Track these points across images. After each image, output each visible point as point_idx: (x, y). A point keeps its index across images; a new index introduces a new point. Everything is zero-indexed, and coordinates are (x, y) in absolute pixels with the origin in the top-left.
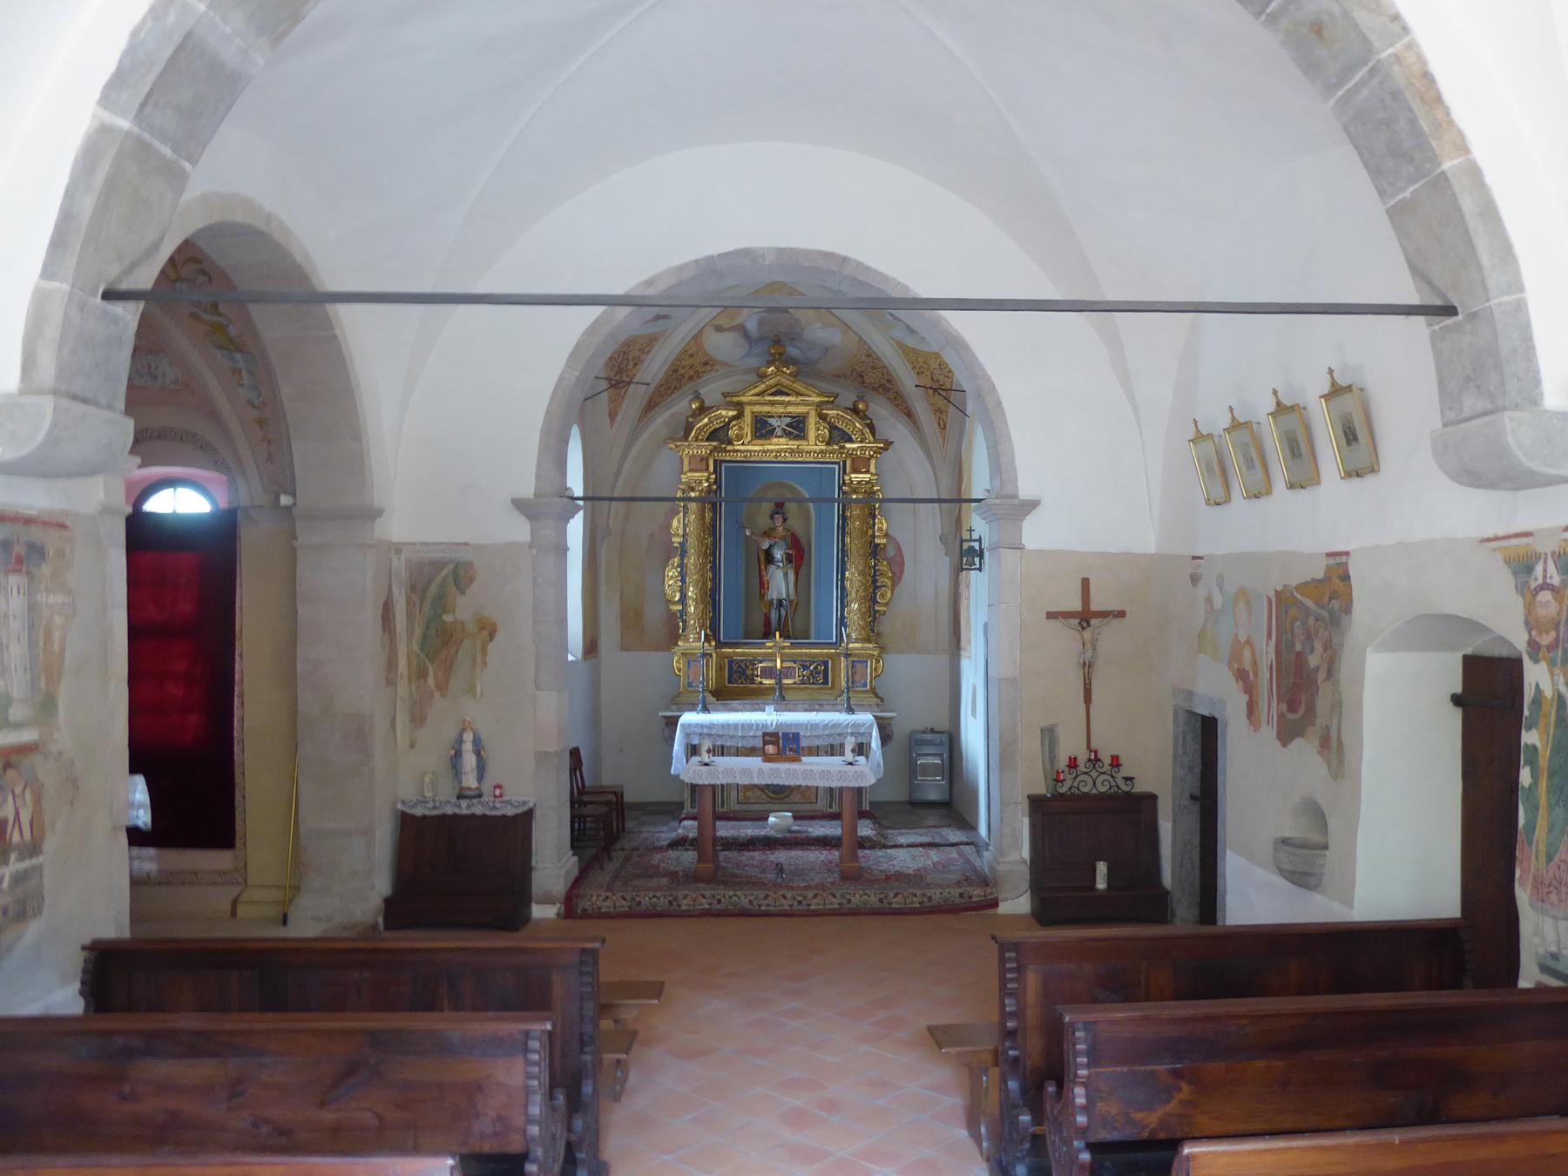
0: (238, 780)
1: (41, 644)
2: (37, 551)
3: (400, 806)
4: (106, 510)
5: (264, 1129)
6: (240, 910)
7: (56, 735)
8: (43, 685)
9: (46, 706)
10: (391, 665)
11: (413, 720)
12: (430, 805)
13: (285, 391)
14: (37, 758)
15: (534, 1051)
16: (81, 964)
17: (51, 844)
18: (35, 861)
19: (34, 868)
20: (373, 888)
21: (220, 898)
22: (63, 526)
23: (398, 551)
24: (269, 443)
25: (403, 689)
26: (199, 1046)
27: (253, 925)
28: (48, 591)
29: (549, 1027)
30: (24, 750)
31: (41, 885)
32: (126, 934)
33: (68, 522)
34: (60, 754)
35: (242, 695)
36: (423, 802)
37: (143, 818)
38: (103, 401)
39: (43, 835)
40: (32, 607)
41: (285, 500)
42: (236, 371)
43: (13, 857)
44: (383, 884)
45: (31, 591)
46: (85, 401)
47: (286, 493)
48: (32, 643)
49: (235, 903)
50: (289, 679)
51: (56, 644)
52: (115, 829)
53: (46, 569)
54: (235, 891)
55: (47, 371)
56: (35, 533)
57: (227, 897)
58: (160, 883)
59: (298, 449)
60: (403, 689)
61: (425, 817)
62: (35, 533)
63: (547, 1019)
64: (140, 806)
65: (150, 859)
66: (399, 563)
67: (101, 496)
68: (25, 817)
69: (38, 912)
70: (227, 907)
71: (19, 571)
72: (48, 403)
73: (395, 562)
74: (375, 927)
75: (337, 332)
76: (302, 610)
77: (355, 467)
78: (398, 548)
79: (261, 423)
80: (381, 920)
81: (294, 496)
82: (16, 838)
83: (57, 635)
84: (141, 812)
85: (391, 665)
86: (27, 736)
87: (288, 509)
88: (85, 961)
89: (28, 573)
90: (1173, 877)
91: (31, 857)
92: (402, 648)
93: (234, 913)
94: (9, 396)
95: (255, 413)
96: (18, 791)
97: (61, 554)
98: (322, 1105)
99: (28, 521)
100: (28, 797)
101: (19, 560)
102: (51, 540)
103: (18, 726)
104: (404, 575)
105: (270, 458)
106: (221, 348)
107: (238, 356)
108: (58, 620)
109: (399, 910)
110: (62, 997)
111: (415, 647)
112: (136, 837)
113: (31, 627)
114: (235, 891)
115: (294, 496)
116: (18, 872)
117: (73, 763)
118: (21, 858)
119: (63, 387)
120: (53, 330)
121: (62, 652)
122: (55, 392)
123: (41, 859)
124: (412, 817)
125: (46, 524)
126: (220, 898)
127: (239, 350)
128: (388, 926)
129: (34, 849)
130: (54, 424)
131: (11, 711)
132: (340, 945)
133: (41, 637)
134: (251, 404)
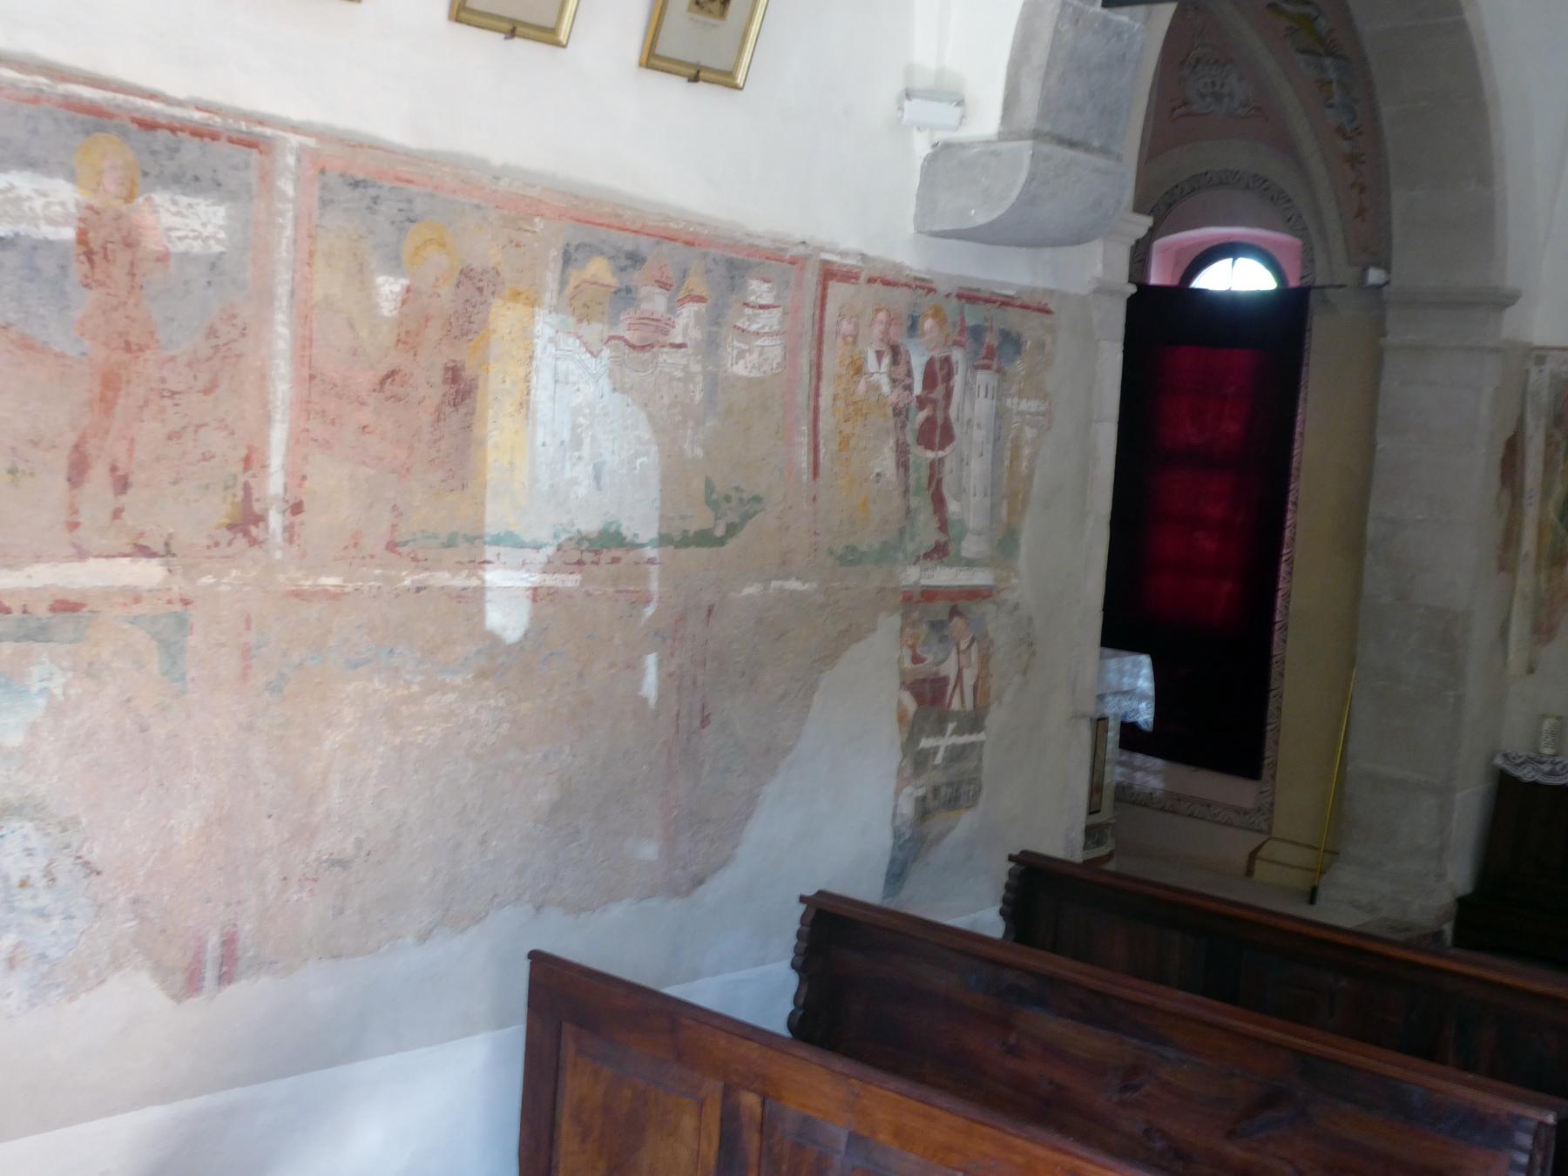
0: (1274, 684)
1: (1007, 463)
2: (1012, 342)
3: (1499, 761)
4: (1102, 290)
5: (1159, 1145)
6: (1260, 867)
7: (1014, 581)
8: (1004, 511)
9: (1006, 542)
10: (1510, 538)
11: (1536, 629)
12: (1547, 768)
13: (1387, 110)
14: (987, 608)
15: (1521, 1149)
16: (1005, 879)
17: (996, 718)
18: (974, 738)
19: (973, 744)
20: (1441, 876)
21: (1236, 845)
22: (1045, 311)
23: (1541, 360)
24: (1363, 189)
25: (1525, 580)
26: (1096, 1010)
27: (1271, 891)
28: (1021, 394)
29: (1551, 1119)
30: (975, 594)
31: (978, 769)
32: (1078, 856)
33: (1051, 306)
34: (1016, 607)
35: (1290, 562)
36: (1536, 760)
37: (1144, 714)
38: (1096, 143)
39: (987, 707)
40: (1000, 415)
41: (1375, 276)
42: (1324, 84)
43: (951, 726)
44: (1459, 875)
45: (1000, 394)
46: (1072, 144)
47: (1378, 265)
48: (996, 460)
49: (1253, 856)
50: (1354, 543)
51: (1025, 464)
52: (1077, 716)
53: (1019, 367)
54: (1255, 840)
55: (1029, 112)
56: (1012, 319)
57: (1219, 842)
58: (1162, 809)
59: (1399, 200)
60: (1525, 580)
61: (1535, 784)
62: (1012, 319)
63: (1551, 1107)
64: (1142, 697)
65: (1156, 773)
66: (1540, 379)
67: (1098, 270)
68: (969, 678)
69: (973, 802)
70: (1242, 860)
71: (987, 367)
72: (1025, 148)
73: (1533, 377)
74: (1437, 935)
75: (1468, 15)
76: (1384, 443)
77: (1479, 222)
78: (1540, 355)
79: (1353, 160)
80: (1448, 928)
81: (1388, 269)
82: (956, 705)
83: (1026, 451)
84: (1143, 705)
85: (1510, 538)
86: (980, 578)
87: (1378, 288)
88: (1010, 873)
89: (999, 371)
90: (643, 671)
91: (971, 733)
92: (1531, 513)
93: (1249, 872)
94: (988, 142)
95: (1345, 146)
96: (963, 646)
97: (1040, 346)
98: (1231, 1135)
99: (1006, 303)
100: (974, 656)
101: (991, 353)
102: (1030, 328)
103: (970, 564)
104: (1545, 397)
105: (1361, 213)
106: (1303, 52)
107: (1328, 61)
108: (1029, 433)
109: (1478, 918)
110: (981, 913)
111: (1553, 516)
112: (1131, 736)
113: (997, 439)
114: (1255, 840)
115: (1388, 269)
116: (954, 746)
117: (1030, 619)
118: (959, 731)
119: (1047, 128)
120: (1039, 54)
121: (1030, 477)
122: (1036, 135)
123: (981, 737)
124: (1516, 781)
125: (1024, 307)
126: (1236, 845)
127: (1329, 54)
128: (1459, 941)
129: (974, 722)
130: (1032, 178)
131: (964, 544)
132: (1341, 938)
133: (1008, 454)
134: (1340, 131)
